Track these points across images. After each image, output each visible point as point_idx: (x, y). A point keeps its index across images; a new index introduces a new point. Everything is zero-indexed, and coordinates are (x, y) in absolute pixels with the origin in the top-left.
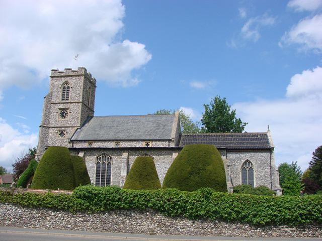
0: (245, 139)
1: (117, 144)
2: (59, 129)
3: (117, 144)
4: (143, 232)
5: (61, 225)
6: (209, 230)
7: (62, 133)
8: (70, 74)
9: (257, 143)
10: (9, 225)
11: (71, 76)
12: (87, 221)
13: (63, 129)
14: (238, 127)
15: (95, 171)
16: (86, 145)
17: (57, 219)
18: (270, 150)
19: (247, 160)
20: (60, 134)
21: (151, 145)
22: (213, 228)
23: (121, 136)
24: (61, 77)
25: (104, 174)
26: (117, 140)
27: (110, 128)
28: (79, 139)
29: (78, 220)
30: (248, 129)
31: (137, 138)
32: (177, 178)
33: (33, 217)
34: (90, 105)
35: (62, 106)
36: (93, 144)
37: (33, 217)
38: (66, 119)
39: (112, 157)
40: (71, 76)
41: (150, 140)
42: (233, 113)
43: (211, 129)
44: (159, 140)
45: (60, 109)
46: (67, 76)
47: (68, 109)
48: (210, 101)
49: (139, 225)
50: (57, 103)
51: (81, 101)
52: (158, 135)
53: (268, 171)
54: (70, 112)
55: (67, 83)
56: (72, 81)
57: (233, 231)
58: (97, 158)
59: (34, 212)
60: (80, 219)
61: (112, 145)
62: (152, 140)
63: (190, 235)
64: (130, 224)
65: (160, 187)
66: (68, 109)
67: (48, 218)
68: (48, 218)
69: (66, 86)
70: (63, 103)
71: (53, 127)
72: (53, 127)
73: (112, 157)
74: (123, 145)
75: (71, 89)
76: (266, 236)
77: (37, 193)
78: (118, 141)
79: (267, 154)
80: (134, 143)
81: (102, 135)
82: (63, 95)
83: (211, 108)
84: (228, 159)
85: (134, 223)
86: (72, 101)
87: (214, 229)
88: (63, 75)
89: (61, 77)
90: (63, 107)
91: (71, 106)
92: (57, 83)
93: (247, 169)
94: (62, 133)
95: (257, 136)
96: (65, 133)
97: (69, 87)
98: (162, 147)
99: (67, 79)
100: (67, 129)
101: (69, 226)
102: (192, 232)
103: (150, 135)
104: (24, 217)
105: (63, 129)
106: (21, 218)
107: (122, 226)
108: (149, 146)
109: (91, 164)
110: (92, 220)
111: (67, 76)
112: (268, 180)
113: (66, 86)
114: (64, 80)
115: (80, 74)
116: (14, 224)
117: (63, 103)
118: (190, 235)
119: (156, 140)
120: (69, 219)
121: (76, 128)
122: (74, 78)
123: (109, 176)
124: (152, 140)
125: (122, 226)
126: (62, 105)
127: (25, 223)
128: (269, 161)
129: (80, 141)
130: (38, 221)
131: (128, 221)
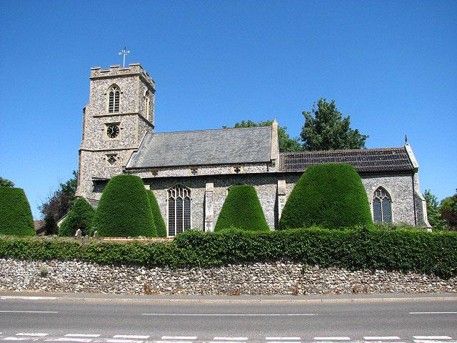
0: (374, 158)
1: (155, 173)
2: (107, 153)
3: (155, 173)
4: (276, 292)
5: (158, 287)
6: (372, 285)
7: (112, 160)
8: (119, 73)
9: (391, 163)
10: (80, 290)
11: (121, 76)
12: (195, 280)
13: (113, 152)
14: (356, 141)
15: (168, 211)
16: (149, 175)
17: (151, 279)
18: (411, 172)
19: (380, 188)
20: (109, 161)
21: (243, 170)
22: (377, 281)
23: (199, 161)
24: (106, 78)
25: (180, 212)
26: (193, 166)
27: (181, 148)
28: (138, 166)
29: (182, 280)
30: (370, 145)
31: (221, 162)
32: (293, 214)
33: (115, 279)
34: (148, 116)
35: (109, 120)
36: (159, 173)
37: (115, 279)
38: (117, 138)
39: (191, 189)
40: (121, 76)
41: (240, 164)
42: (347, 123)
43: (310, 146)
44: (254, 164)
45: (107, 124)
46: (114, 77)
47: (118, 124)
48: (311, 108)
49: (270, 281)
50: (102, 116)
51: (137, 111)
52: (252, 157)
53: (411, 201)
54: (122, 129)
55: (115, 86)
56: (122, 84)
57: (406, 285)
58: (170, 192)
59: (117, 271)
60: (185, 278)
61: (187, 173)
62: (243, 164)
63: (345, 292)
64: (258, 281)
65: (30, 224)
66: (118, 124)
67: (138, 278)
68: (138, 278)
69: (114, 91)
70: (111, 116)
71: (98, 151)
72: (98, 151)
73: (191, 189)
74: (202, 172)
75: (121, 96)
76: (454, 290)
77: (119, 243)
78: (194, 167)
79: (409, 178)
80: (218, 169)
81: (170, 159)
82: (111, 104)
83: (314, 116)
84: (370, 186)
85: (264, 279)
86: (124, 113)
87: (379, 283)
88: (108, 75)
89: (106, 78)
90: (111, 122)
91: (123, 120)
92: (100, 87)
93: (381, 200)
94: (112, 160)
95: (390, 152)
96: (116, 158)
97: (118, 92)
98: (258, 172)
99: (115, 81)
100: (118, 152)
101: (170, 288)
102: (347, 288)
103: (240, 156)
104: (102, 278)
105: (113, 152)
106: (97, 279)
107: (245, 284)
108: (239, 173)
109: (162, 198)
110: (202, 278)
111: (114, 77)
112: (411, 215)
113: (114, 91)
114: (110, 82)
115: (133, 73)
116: (87, 289)
117: (111, 116)
118: (345, 292)
119: (249, 164)
120: (168, 278)
121: (132, 151)
122: (125, 79)
123: (188, 217)
124: (243, 164)
125: (245, 284)
126: (110, 118)
127: (105, 288)
128: (411, 188)
129: (139, 168)
130: (122, 283)
131: (254, 278)
